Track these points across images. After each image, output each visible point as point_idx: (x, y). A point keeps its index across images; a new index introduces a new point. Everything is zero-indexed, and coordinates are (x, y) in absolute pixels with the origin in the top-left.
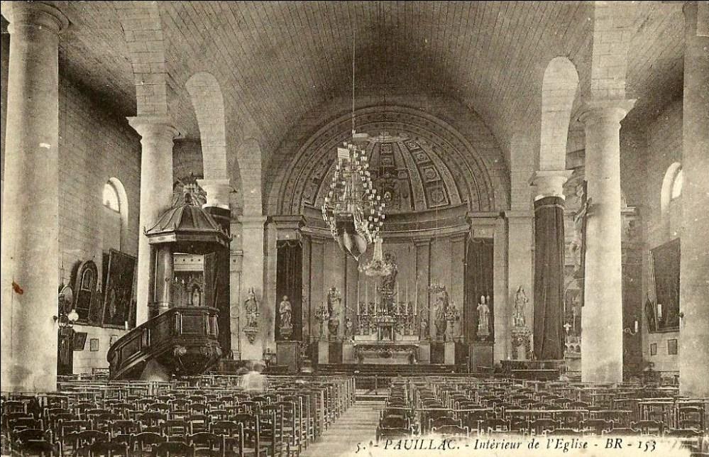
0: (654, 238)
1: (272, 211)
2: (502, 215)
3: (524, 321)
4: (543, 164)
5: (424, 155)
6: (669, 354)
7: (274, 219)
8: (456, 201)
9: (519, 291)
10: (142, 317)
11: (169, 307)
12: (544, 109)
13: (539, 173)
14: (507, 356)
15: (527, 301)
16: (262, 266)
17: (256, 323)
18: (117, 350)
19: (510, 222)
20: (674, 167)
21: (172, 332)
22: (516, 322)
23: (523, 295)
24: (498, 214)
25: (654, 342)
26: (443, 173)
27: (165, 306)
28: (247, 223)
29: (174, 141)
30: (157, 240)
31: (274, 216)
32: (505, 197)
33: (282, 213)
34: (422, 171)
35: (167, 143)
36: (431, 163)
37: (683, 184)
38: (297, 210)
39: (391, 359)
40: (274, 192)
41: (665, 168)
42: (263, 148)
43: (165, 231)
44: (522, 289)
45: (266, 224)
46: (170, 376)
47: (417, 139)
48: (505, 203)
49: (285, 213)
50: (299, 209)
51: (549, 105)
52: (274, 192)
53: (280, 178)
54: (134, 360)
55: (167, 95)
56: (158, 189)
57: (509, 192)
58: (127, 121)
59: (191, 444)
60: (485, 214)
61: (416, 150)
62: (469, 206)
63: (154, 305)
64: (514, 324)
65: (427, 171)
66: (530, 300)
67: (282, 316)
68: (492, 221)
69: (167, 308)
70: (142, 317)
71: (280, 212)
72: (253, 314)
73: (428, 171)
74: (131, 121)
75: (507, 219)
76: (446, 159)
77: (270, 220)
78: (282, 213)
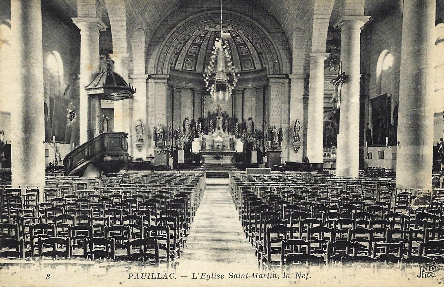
0: (373, 95)
1: (151, 71)
2: (287, 77)
3: (299, 139)
4: (313, 49)
5: (241, 40)
6: (379, 159)
7: (152, 76)
8: (258, 67)
9: (296, 121)
10: (84, 139)
11: (100, 133)
12: (315, 17)
13: (311, 54)
14: (407, 226)
15: (301, 128)
16: (145, 105)
17: (142, 139)
18: (70, 158)
19: (292, 80)
20: (385, 51)
21: (103, 148)
22: (294, 140)
23: (299, 124)
24: (284, 76)
25: (370, 152)
26: (251, 50)
27: (97, 134)
28: (136, 78)
29: (100, 32)
30: (92, 92)
31: (152, 75)
32: (288, 65)
33: (157, 73)
34: (239, 49)
35: (96, 33)
36: (245, 44)
37: (393, 64)
38: (166, 71)
39: (221, 160)
40: (152, 62)
41: (380, 52)
42: (146, 35)
43: (97, 87)
44: (298, 121)
45: (147, 79)
46: (100, 173)
47: (237, 30)
48: (288, 69)
49: (159, 73)
50: (167, 71)
51: (317, 14)
52: (152, 62)
53: (156, 52)
54: (80, 165)
55: (96, 5)
56: (91, 60)
57: (291, 62)
58: (72, 20)
59: (90, 209)
60: (277, 76)
61: (237, 36)
62: (268, 71)
63: (90, 132)
64: (293, 141)
65: (242, 49)
66: (302, 127)
67: (158, 135)
68: (281, 80)
69: (98, 133)
70: (84, 139)
71: (156, 72)
72: (141, 134)
73: (243, 48)
74: (74, 20)
75: (290, 80)
76: (255, 43)
77: (150, 77)
78: (157, 73)
